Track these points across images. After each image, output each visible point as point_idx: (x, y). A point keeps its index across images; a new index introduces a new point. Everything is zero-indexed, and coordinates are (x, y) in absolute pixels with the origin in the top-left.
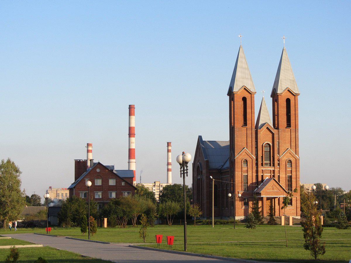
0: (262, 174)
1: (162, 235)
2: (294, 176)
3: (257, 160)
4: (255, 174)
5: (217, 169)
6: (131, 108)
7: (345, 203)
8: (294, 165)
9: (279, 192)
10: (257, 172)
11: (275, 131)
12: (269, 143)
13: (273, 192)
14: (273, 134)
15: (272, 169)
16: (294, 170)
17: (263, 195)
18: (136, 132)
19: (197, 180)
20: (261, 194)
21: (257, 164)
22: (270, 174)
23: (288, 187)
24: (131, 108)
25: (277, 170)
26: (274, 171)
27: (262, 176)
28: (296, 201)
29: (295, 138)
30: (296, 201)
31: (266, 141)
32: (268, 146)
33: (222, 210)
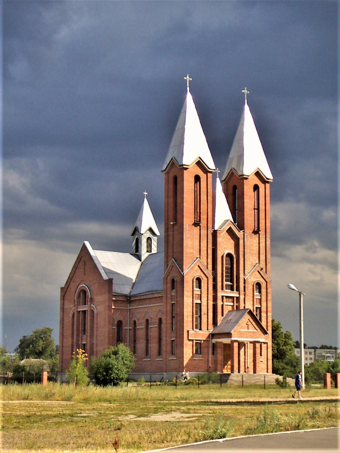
1: (277, 369)
4: (211, 303)
5: (126, 296)
7: (128, 307)
8: (263, 290)
9: (255, 332)
10: (215, 299)
11: (239, 234)
13: (249, 332)
15: (235, 294)
17: (235, 337)
20: (231, 336)
22: (232, 304)
23: (196, 308)
25: (242, 297)
26: (238, 299)
27: (222, 305)
28: (267, 348)
29: (264, 249)
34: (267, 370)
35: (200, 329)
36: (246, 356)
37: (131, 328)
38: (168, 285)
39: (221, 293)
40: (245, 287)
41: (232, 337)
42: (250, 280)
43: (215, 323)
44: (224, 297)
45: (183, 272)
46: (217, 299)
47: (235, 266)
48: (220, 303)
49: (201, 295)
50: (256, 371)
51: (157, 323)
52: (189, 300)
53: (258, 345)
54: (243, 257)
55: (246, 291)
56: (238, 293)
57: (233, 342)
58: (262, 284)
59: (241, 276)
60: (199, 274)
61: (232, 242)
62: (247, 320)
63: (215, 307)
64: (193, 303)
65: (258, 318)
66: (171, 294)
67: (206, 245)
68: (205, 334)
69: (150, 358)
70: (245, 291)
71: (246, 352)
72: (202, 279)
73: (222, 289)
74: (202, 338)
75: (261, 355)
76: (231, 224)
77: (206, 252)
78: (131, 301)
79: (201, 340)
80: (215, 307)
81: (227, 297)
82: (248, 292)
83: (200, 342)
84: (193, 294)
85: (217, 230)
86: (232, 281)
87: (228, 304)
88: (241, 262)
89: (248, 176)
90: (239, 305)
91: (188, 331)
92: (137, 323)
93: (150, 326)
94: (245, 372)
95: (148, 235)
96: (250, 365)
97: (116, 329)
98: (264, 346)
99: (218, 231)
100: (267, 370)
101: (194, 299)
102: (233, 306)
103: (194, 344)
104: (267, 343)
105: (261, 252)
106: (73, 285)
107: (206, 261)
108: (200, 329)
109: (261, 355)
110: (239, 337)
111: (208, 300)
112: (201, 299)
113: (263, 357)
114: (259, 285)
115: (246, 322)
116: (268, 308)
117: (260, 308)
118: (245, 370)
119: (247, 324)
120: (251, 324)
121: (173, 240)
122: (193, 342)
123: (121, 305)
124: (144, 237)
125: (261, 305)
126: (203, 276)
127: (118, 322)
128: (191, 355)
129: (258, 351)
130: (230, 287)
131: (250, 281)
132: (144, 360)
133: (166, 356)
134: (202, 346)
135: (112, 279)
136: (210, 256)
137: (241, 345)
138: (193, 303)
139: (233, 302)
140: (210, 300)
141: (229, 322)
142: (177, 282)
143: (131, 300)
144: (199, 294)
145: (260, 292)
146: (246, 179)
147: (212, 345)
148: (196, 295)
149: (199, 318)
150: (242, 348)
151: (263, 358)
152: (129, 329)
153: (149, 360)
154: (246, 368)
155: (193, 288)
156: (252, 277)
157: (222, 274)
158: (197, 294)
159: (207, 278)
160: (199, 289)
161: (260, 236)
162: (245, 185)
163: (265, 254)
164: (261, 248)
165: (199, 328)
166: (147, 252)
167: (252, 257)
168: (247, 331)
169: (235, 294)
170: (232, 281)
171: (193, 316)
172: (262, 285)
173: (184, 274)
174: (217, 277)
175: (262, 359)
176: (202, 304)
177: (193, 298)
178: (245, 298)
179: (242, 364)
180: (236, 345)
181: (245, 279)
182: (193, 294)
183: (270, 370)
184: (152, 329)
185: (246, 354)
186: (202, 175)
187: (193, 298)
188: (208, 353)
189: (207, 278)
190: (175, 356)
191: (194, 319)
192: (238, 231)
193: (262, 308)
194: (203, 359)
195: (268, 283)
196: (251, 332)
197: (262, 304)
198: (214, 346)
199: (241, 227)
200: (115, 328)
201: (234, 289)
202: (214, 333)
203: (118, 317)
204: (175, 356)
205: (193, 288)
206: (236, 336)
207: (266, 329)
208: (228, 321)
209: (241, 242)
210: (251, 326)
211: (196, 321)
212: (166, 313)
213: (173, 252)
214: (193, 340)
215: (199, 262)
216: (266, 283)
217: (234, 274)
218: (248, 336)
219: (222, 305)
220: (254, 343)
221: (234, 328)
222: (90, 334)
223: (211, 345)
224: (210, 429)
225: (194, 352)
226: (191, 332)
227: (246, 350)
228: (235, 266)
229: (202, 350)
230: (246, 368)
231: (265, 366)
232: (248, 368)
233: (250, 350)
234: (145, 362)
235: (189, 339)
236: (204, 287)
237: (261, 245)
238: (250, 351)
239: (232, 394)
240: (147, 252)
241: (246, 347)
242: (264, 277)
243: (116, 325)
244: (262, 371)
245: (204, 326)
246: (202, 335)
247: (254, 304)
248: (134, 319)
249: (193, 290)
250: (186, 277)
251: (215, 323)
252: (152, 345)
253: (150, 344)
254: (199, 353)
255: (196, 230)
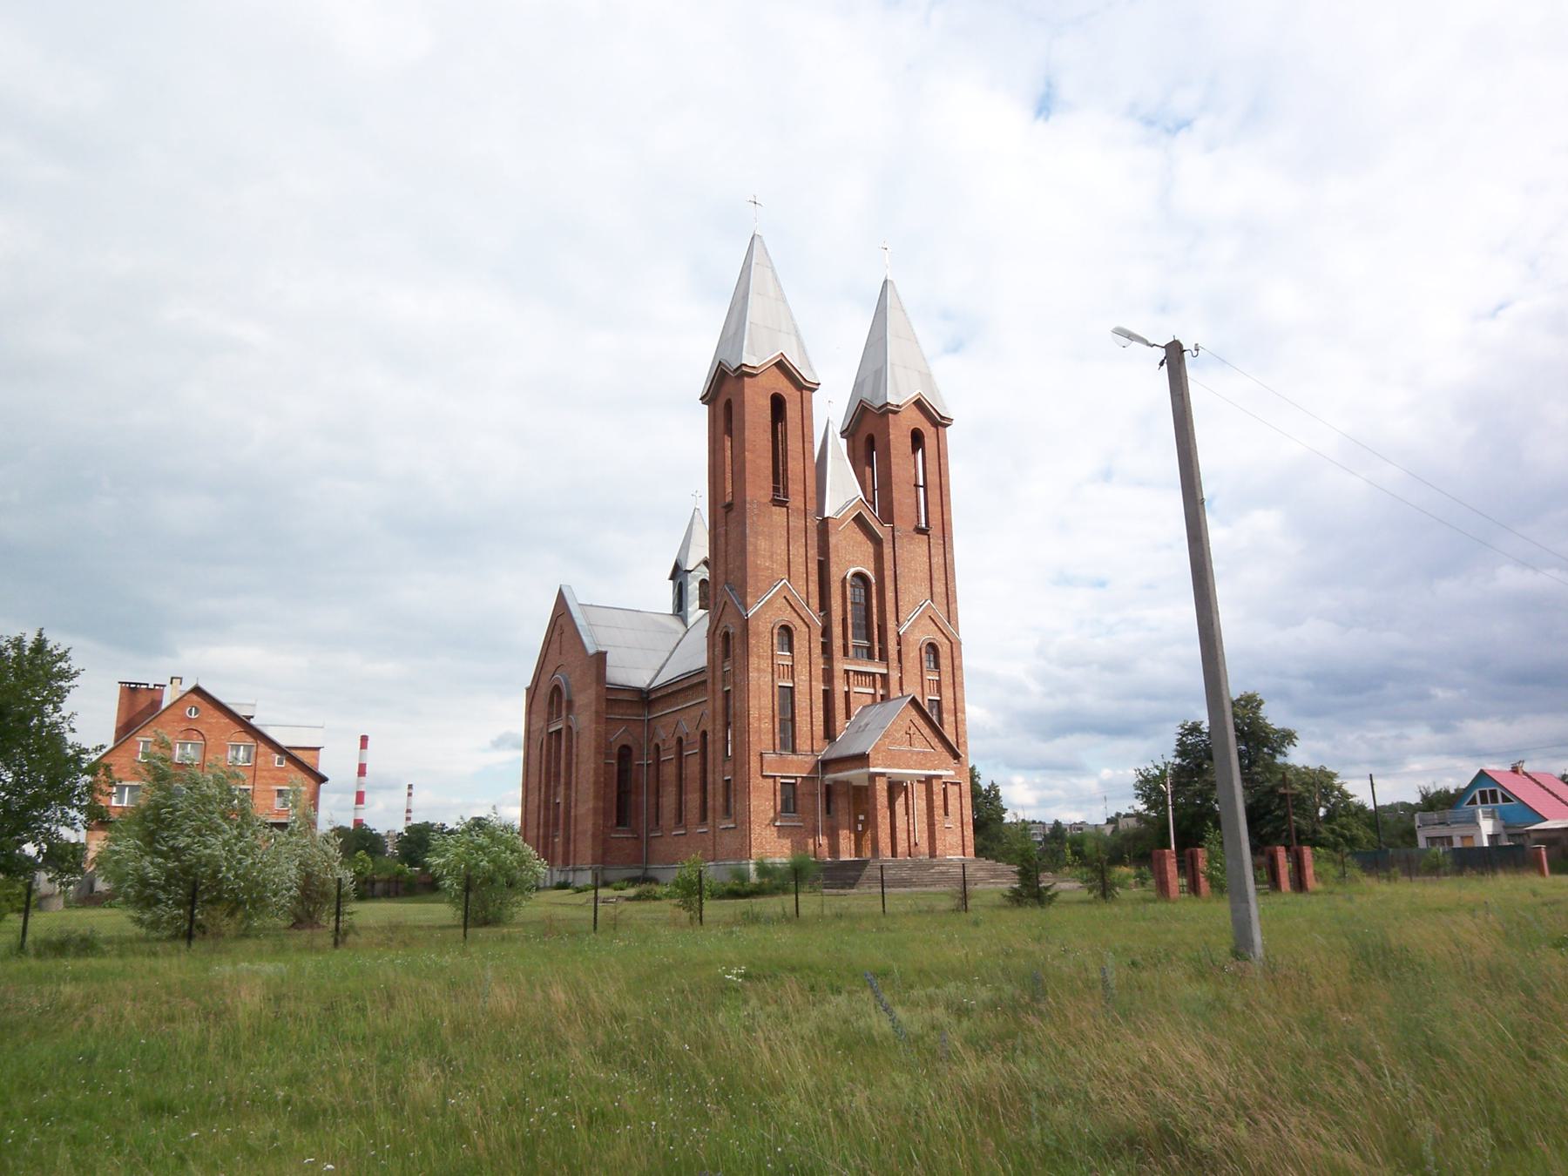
0: (846, 689)
2: (947, 704)
3: (826, 632)
4: (819, 687)
5: (639, 691)
6: (364, 739)
8: (945, 662)
10: (828, 676)
11: (881, 530)
12: (864, 570)
14: (877, 542)
15: (877, 668)
16: (946, 680)
18: (368, 770)
19: (549, 743)
21: (827, 649)
24: (364, 739)
25: (894, 676)
26: (885, 677)
27: (847, 694)
28: (961, 796)
29: (942, 569)
30: (961, 796)
31: (853, 563)
32: (861, 584)
33: (647, 837)
34: (964, 849)
35: (794, 751)
36: (911, 816)
37: (650, 762)
38: (716, 649)
39: (843, 663)
40: (899, 652)
41: (870, 765)
42: (911, 638)
43: (829, 734)
44: (851, 674)
45: (746, 610)
46: (833, 676)
47: (874, 602)
48: (840, 687)
49: (792, 666)
50: (846, 695)
51: (698, 745)
52: (762, 679)
53: (937, 787)
54: (893, 583)
55: (903, 662)
56: (885, 665)
57: (873, 776)
58: (939, 647)
59: (891, 624)
60: (787, 616)
61: (869, 548)
62: (908, 721)
63: (828, 696)
64: (773, 687)
65: (935, 718)
66: (723, 668)
67: (803, 555)
68: (805, 762)
69: (685, 827)
70: (900, 661)
71: (911, 807)
72: (793, 629)
73: (846, 654)
74: (796, 773)
75: (946, 814)
76: (862, 508)
77: (803, 569)
78: (652, 701)
79: (795, 778)
80: (828, 696)
81: (857, 673)
82: (909, 664)
83: (793, 781)
84: (773, 664)
85: (828, 518)
86: (869, 637)
87: (862, 689)
88: (889, 595)
89: (898, 406)
90: (889, 692)
91: (762, 754)
92: (661, 749)
93: (685, 753)
94: (910, 856)
95: (700, 575)
96: (921, 837)
97: (616, 765)
98: (952, 790)
99: (830, 520)
100: (964, 849)
101: (776, 676)
102: (874, 695)
103: (778, 786)
104: (960, 783)
105: (935, 576)
106: (545, 678)
107: (803, 589)
108: (794, 751)
109: (946, 814)
110: (889, 766)
111: (811, 681)
112: (793, 679)
113: (951, 817)
114: (933, 648)
115: (905, 728)
116: (957, 701)
117: (939, 702)
118: (910, 850)
119: (906, 733)
120: (918, 733)
121: (727, 544)
122: (775, 782)
123: (629, 711)
124: (692, 577)
125: (941, 696)
126: (798, 622)
127: (620, 748)
128: (772, 815)
129: (938, 801)
130: (865, 651)
131: (911, 639)
132: (674, 833)
133: (714, 821)
134: (799, 792)
135: (605, 653)
136: (814, 577)
137: (896, 788)
138: (773, 687)
139: (874, 687)
140: (817, 681)
141: (863, 730)
142: (733, 638)
143: (650, 699)
144: (787, 665)
145: (937, 666)
146: (895, 413)
147: (824, 789)
148: (781, 668)
149: (790, 723)
150: (899, 797)
151: (952, 822)
152: (647, 764)
153: (683, 832)
154: (912, 844)
155: (772, 650)
156: (917, 631)
157: (844, 620)
158: (783, 665)
159: (809, 627)
160: (788, 654)
161: (931, 540)
162: (891, 427)
163: (944, 582)
164: (934, 566)
165: (791, 749)
166: (700, 608)
167: (915, 586)
168: (909, 751)
169: (877, 668)
170: (869, 637)
171: (774, 717)
172: (940, 650)
173: (749, 616)
174: (831, 627)
175: (949, 823)
176: (796, 690)
177: (773, 675)
178: (901, 678)
179: (901, 836)
180: (881, 786)
181: (901, 633)
182: (773, 664)
183: (971, 850)
184: (690, 758)
185: (911, 811)
186: (790, 395)
187: (773, 675)
188: (816, 809)
189: (809, 627)
190: (733, 819)
191: (777, 726)
192: (878, 524)
193: (944, 702)
194: (801, 824)
195: (954, 646)
196: (919, 753)
197: (943, 693)
198: (829, 791)
199: (887, 516)
200: (612, 763)
201: (874, 655)
202: (827, 757)
203: (619, 736)
204: (733, 819)
205: (772, 650)
206: (879, 762)
207: (955, 746)
208: (860, 727)
209: (887, 550)
210: (917, 738)
211: (781, 731)
212: (714, 717)
213: (726, 573)
214: (774, 777)
215: (786, 590)
216: (949, 644)
217: (872, 622)
218: (912, 763)
219: (847, 694)
220: (929, 780)
221: (745, 524)
222: (565, 779)
223: (820, 790)
224: (461, 1132)
225: (779, 808)
226: (769, 757)
227: (910, 802)
228: (874, 602)
229: (799, 802)
230: (912, 844)
231: (957, 839)
232: (916, 844)
233: (920, 801)
234: (676, 839)
235: (764, 774)
236: (799, 648)
237: (934, 560)
238: (920, 804)
239: (1559, 1060)
240: (700, 608)
241: (910, 796)
242: (945, 631)
243: (616, 756)
244: (951, 852)
245: (803, 744)
246: (797, 767)
247: (925, 693)
248: (656, 741)
249: (773, 655)
250: (754, 623)
251: (829, 734)
252: (690, 796)
253: (686, 794)
254: (792, 810)
255: (779, 513)
